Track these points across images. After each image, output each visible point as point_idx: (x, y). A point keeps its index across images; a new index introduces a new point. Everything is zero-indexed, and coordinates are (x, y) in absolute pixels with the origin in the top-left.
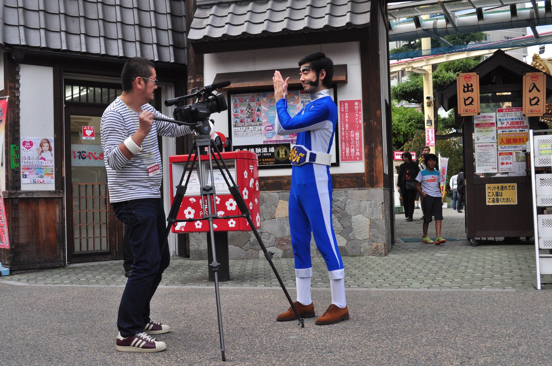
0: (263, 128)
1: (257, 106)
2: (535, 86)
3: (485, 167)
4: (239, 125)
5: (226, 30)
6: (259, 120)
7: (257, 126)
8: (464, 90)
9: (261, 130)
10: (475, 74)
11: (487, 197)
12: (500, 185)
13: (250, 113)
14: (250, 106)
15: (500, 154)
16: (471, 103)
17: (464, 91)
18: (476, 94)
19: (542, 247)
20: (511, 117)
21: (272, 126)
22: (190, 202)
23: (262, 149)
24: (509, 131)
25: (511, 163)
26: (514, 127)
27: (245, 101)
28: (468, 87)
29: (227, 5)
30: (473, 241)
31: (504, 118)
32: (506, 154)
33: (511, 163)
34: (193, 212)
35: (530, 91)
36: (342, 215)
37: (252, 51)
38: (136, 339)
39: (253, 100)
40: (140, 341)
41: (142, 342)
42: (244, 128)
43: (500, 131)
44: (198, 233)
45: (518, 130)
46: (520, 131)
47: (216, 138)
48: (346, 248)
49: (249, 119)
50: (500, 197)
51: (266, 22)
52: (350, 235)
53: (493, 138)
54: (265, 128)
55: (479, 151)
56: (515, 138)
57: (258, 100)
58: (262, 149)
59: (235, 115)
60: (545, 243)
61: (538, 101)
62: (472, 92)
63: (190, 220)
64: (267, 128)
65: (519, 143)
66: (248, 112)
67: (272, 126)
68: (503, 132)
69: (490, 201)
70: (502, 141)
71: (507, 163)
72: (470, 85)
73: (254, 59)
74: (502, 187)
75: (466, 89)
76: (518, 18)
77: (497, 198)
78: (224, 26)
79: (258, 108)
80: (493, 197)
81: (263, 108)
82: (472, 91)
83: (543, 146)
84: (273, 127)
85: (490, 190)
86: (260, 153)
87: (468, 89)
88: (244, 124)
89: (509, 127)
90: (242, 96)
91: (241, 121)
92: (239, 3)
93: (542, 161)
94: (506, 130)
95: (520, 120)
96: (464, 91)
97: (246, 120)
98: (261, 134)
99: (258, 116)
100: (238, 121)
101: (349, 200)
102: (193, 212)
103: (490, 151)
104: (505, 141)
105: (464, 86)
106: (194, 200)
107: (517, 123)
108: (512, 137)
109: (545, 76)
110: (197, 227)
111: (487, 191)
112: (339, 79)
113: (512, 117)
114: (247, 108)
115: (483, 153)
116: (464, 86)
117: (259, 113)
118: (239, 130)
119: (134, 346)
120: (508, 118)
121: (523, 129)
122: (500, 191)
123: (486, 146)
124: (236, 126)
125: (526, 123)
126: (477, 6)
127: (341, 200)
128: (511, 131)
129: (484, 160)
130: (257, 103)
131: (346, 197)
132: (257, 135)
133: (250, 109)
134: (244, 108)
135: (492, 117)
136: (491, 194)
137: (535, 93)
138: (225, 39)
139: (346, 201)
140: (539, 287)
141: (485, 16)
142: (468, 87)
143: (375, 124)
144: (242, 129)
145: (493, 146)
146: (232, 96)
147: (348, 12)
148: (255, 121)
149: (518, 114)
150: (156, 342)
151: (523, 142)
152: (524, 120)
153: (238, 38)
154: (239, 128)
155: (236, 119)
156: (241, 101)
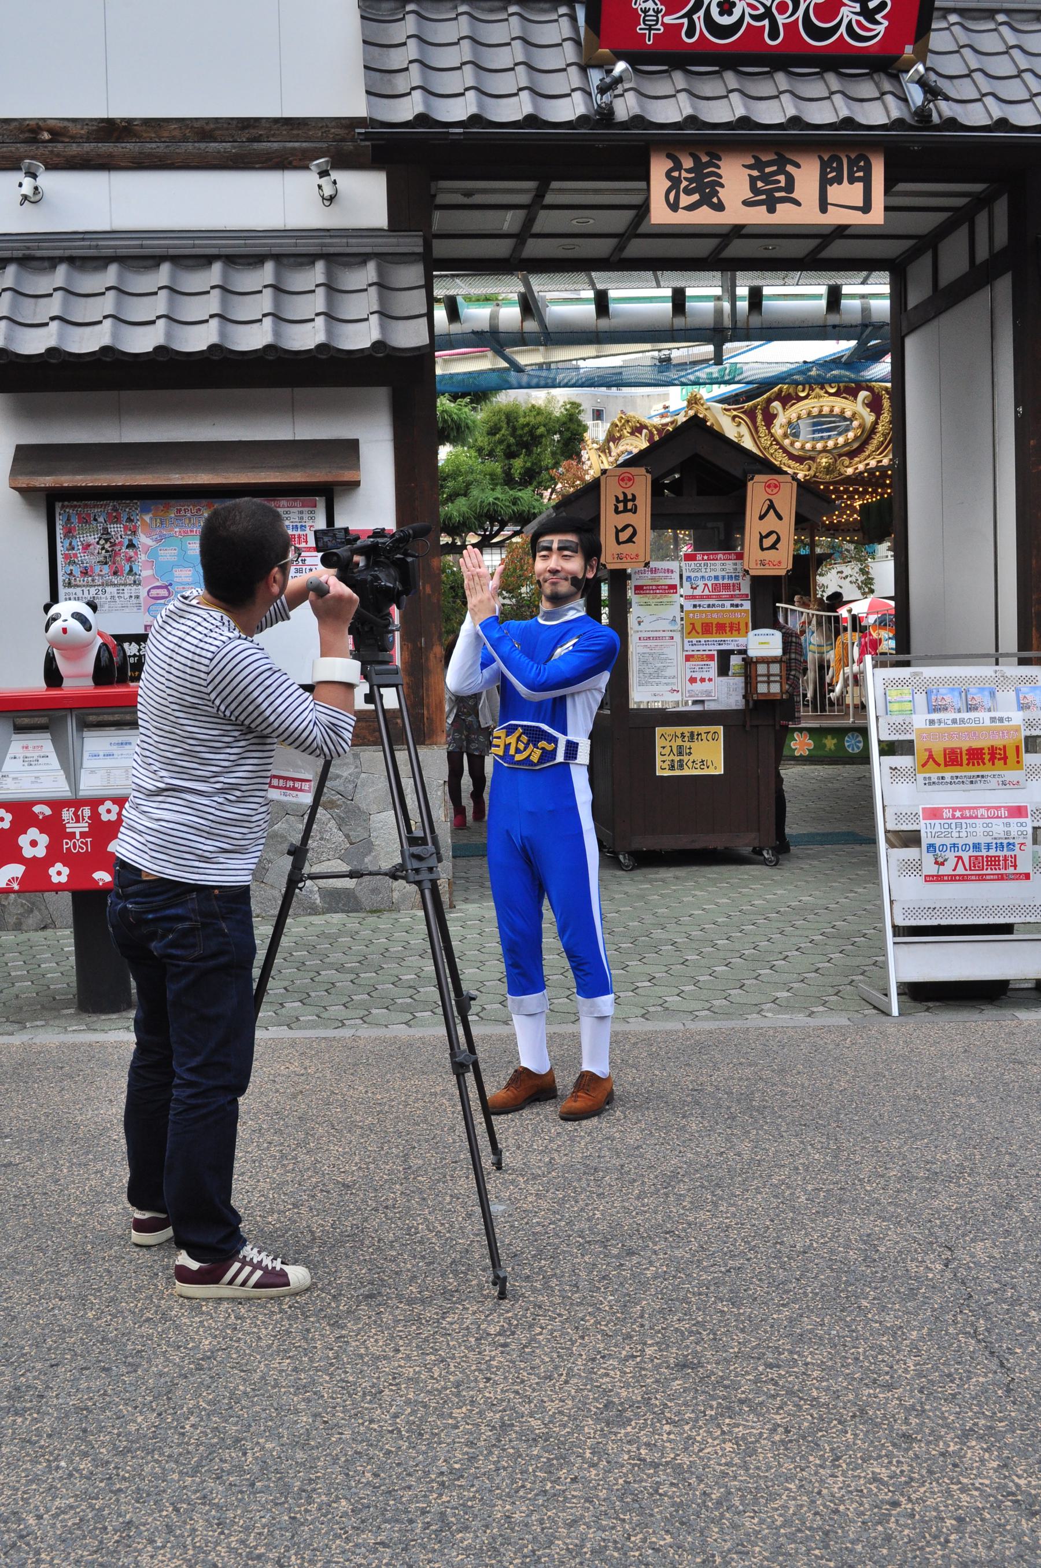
0: (143, 592)
1: (126, 534)
2: (771, 506)
3: (655, 689)
4: (78, 583)
5: (55, 337)
6: (131, 570)
7: (128, 587)
8: (616, 508)
9: (138, 597)
10: (642, 470)
11: (658, 759)
12: (687, 730)
13: (107, 551)
14: (108, 533)
15: (688, 658)
16: (773, 547)
17: (617, 511)
18: (642, 519)
19: (900, 922)
20: (713, 574)
21: (166, 587)
22: (36, 816)
23: (140, 645)
24: (709, 606)
25: (710, 680)
26: (719, 598)
27: (95, 520)
28: (626, 501)
29: (46, 264)
30: (625, 858)
31: (699, 575)
32: (702, 658)
33: (710, 680)
34: (43, 840)
35: (761, 518)
36: (346, 813)
37: (114, 394)
38: (237, 1265)
39: (117, 520)
40: (248, 1269)
41: (252, 1273)
42: (93, 590)
43: (688, 605)
44: (54, 893)
45: (728, 603)
46: (732, 605)
47: (100, 647)
48: (356, 893)
49: (106, 567)
50: (685, 758)
51: (161, 322)
52: (366, 860)
53: (674, 620)
54: (149, 591)
55: (641, 650)
56: (721, 622)
57: (130, 520)
58: (140, 645)
59: (66, 557)
60: (907, 911)
61: (778, 540)
62: (635, 512)
63: (32, 864)
64: (154, 592)
65: (729, 633)
66: (103, 548)
67: (166, 587)
68: (695, 606)
69: (666, 765)
70: (694, 628)
71: (703, 680)
72: (630, 497)
73: (119, 413)
74: (692, 734)
75: (621, 506)
76: (688, 319)
77: (680, 761)
78: (47, 324)
79: (130, 540)
80: (672, 757)
81: (143, 539)
82: (634, 510)
83: (893, 694)
84: (168, 590)
85: (665, 739)
86: (135, 656)
87: (625, 506)
88: (93, 580)
89: (708, 597)
90: (86, 506)
91: (85, 573)
92: (78, 263)
93: (894, 727)
94: (702, 603)
95: (734, 581)
96: (617, 511)
97: (97, 569)
98: (139, 606)
99: (129, 559)
100: (77, 571)
101: (363, 775)
102: (43, 840)
103: (665, 651)
104: (699, 630)
105: (617, 498)
106: (48, 811)
107: (726, 587)
108: (715, 618)
109: (795, 484)
110: (55, 879)
111: (659, 743)
112: (346, 479)
113: (716, 574)
114: (100, 538)
115: (650, 654)
116: (617, 498)
117: (131, 552)
118: (80, 594)
119: (231, 1282)
120: (706, 575)
121: (739, 602)
122: (687, 744)
123: (657, 638)
124: (69, 583)
125: (746, 589)
126: (600, 286)
127: (345, 774)
128: (714, 605)
129: (652, 671)
130: (125, 528)
131: (356, 767)
132: (127, 610)
133: (107, 540)
134: (92, 539)
135: (672, 572)
136: (667, 751)
137: (771, 522)
138: (53, 361)
139: (358, 778)
140: (895, 1011)
141: (612, 306)
142: (626, 501)
143: (428, 590)
144: (86, 592)
145: (672, 638)
146: (58, 506)
147: (372, 313)
148: (122, 571)
149: (730, 565)
150: (287, 1269)
151: (739, 630)
152: (741, 581)
153: (88, 359)
154: (78, 590)
155: (71, 567)
156: (85, 521)
